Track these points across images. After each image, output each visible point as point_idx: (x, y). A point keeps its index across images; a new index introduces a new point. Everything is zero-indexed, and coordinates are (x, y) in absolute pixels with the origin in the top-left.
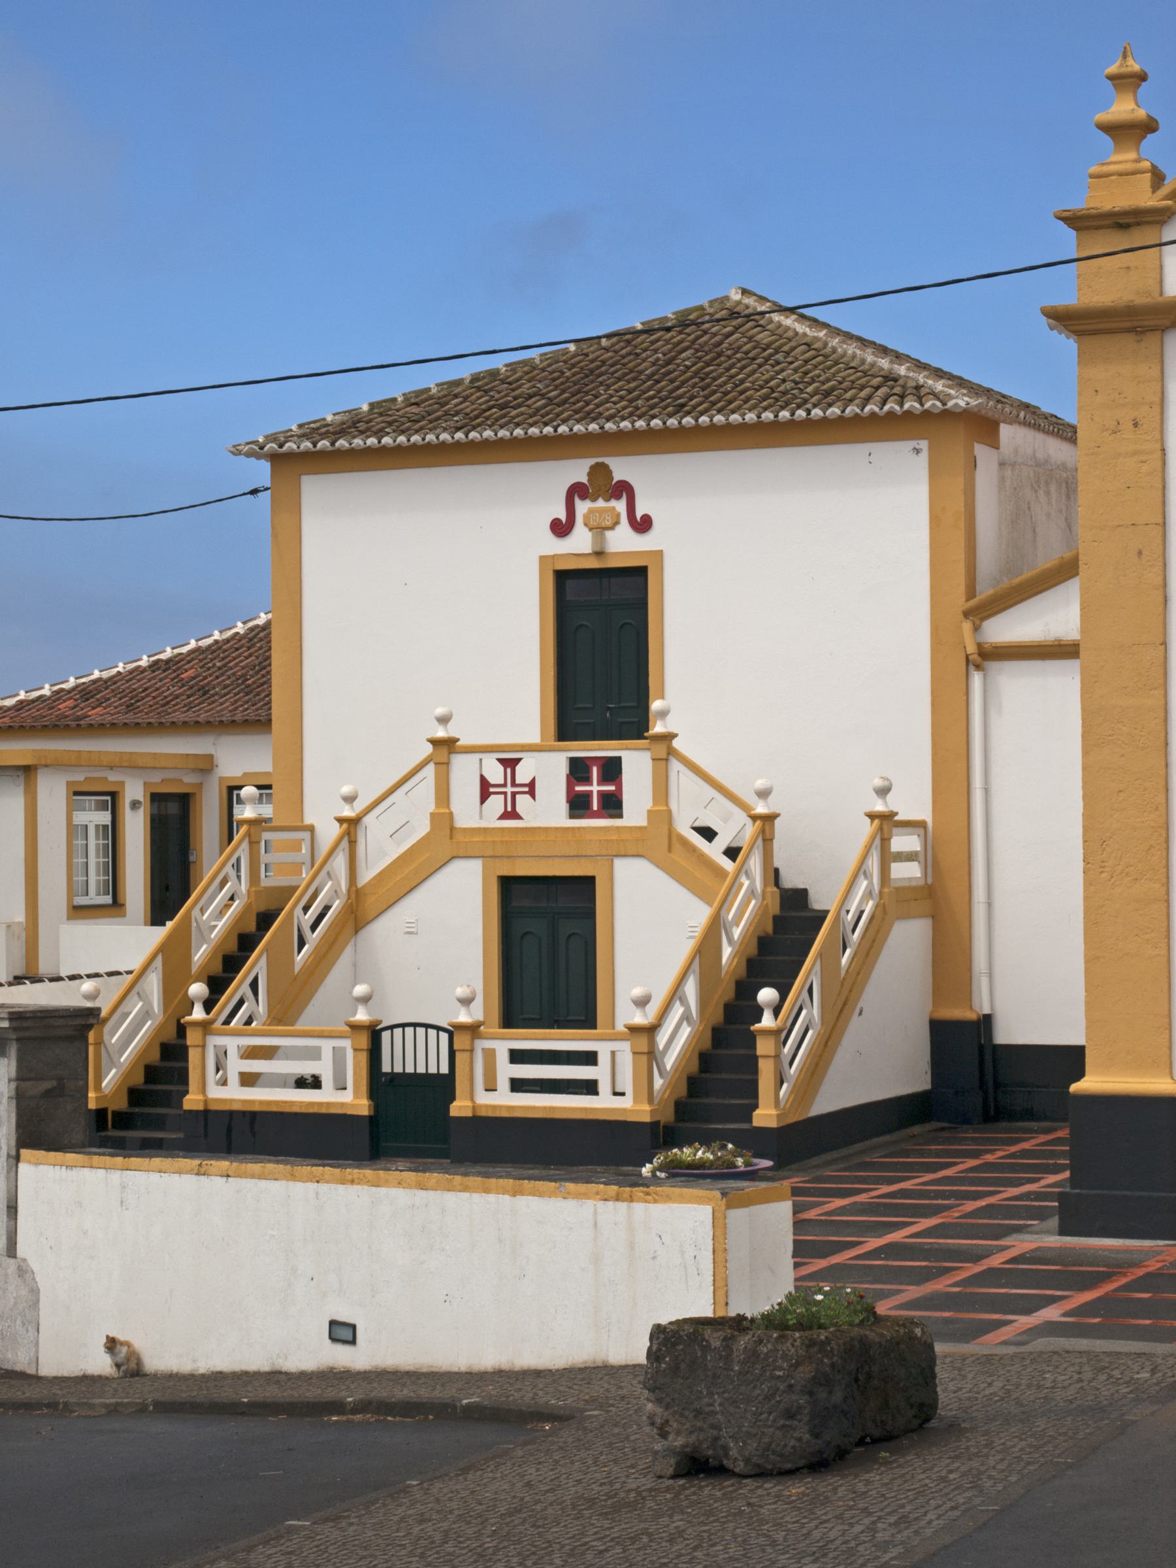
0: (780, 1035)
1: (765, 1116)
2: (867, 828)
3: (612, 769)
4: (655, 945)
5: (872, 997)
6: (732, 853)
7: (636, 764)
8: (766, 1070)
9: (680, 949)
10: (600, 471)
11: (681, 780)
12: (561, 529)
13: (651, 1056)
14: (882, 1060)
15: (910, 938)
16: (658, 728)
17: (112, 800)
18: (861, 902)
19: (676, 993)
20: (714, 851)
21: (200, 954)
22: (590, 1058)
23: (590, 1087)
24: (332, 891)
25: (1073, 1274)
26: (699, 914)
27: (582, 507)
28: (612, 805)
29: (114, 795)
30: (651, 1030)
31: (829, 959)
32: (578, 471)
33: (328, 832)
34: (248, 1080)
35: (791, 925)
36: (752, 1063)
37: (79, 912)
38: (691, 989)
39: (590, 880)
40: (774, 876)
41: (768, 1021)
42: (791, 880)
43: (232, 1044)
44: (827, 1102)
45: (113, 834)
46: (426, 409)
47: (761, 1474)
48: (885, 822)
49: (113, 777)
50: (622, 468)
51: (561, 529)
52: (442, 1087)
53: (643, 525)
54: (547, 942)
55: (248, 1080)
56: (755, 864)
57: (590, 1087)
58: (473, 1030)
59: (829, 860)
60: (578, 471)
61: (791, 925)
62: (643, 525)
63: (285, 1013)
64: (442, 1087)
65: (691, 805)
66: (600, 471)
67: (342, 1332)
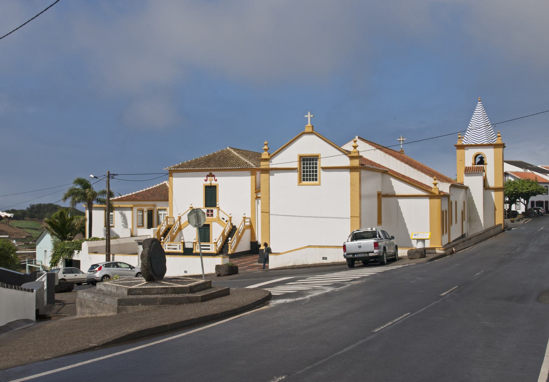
0: (231, 243)
1: (229, 252)
2: (243, 219)
3: (212, 211)
4: (217, 233)
5: (242, 239)
6: (227, 221)
7: (215, 210)
8: (230, 247)
9: (220, 233)
10: (211, 174)
11: (221, 213)
12: (206, 181)
13: (217, 246)
14: (245, 246)
15: (248, 232)
16: (217, 206)
17: (143, 211)
18: (242, 227)
19: (220, 238)
20: (224, 221)
21: (161, 233)
22: (209, 246)
23: (209, 249)
24: (177, 226)
25: (258, 266)
26: (222, 229)
27: (208, 178)
28: (212, 215)
29: (143, 211)
30: (216, 243)
31: (237, 234)
32: (208, 173)
33: (176, 219)
34: (168, 248)
35: (233, 230)
36: (228, 246)
37: (138, 227)
38: (221, 238)
39: (209, 225)
40: (232, 224)
41: (230, 242)
42: (234, 225)
43: (167, 244)
44: (237, 251)
45: (143, 215)
46: (190, 164)
47: (224, 276)
48: (245, 218)
49: (143, 208)
50: (213, 173)
51: (206, 181)
52: (192, 249)
53: (216, 180)
54: (204, 233)
55: (168, 248)
56: (229, 223)
57: (209, 249)
58: (196, 243)
59: (238, 223)
60: (208, 173)
61: (233, 230)
62: (216, 180)
63: (172, 240)
64: (192, 249)
65: (221, 215)
66: (211, 174)
67: (186, 272)
